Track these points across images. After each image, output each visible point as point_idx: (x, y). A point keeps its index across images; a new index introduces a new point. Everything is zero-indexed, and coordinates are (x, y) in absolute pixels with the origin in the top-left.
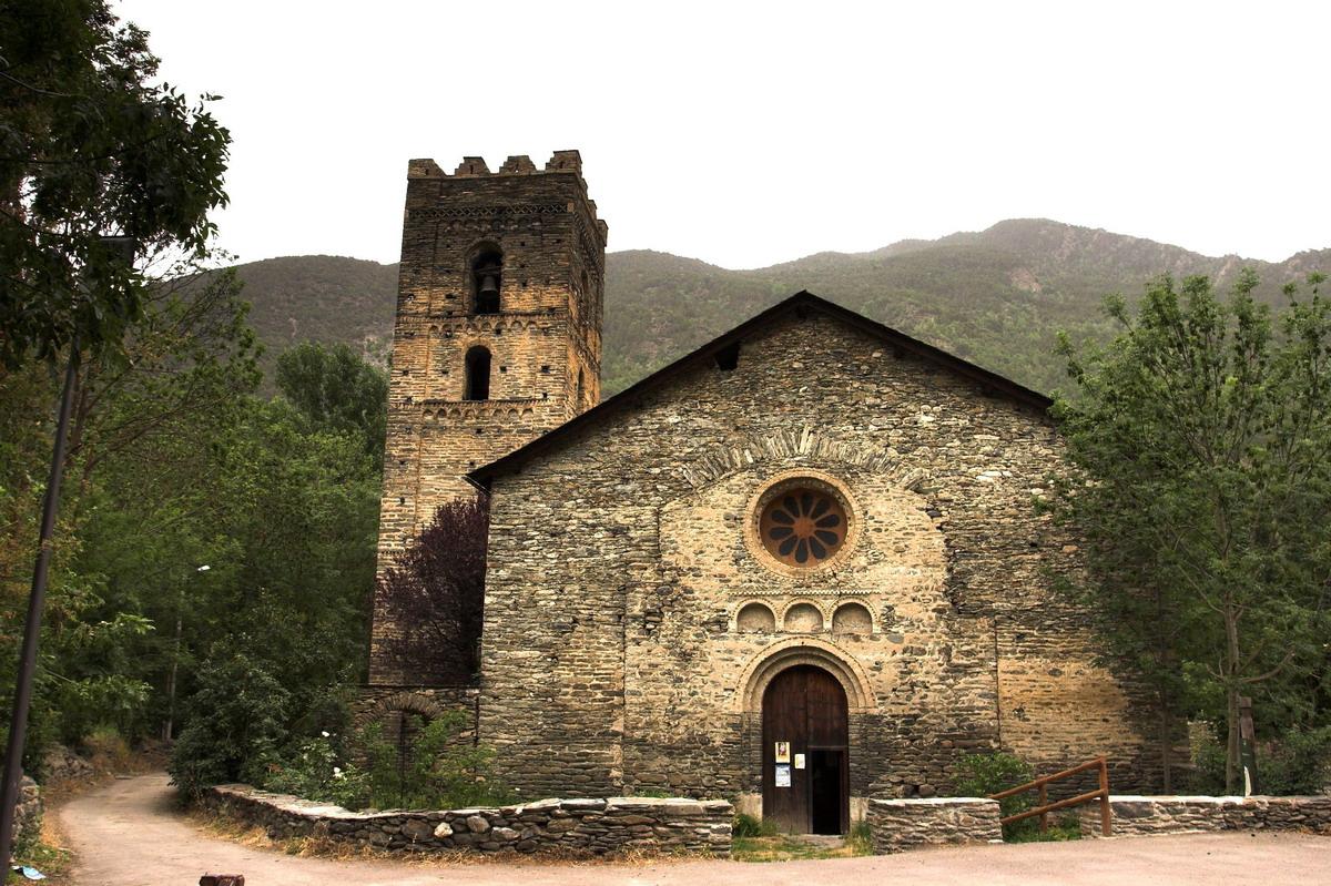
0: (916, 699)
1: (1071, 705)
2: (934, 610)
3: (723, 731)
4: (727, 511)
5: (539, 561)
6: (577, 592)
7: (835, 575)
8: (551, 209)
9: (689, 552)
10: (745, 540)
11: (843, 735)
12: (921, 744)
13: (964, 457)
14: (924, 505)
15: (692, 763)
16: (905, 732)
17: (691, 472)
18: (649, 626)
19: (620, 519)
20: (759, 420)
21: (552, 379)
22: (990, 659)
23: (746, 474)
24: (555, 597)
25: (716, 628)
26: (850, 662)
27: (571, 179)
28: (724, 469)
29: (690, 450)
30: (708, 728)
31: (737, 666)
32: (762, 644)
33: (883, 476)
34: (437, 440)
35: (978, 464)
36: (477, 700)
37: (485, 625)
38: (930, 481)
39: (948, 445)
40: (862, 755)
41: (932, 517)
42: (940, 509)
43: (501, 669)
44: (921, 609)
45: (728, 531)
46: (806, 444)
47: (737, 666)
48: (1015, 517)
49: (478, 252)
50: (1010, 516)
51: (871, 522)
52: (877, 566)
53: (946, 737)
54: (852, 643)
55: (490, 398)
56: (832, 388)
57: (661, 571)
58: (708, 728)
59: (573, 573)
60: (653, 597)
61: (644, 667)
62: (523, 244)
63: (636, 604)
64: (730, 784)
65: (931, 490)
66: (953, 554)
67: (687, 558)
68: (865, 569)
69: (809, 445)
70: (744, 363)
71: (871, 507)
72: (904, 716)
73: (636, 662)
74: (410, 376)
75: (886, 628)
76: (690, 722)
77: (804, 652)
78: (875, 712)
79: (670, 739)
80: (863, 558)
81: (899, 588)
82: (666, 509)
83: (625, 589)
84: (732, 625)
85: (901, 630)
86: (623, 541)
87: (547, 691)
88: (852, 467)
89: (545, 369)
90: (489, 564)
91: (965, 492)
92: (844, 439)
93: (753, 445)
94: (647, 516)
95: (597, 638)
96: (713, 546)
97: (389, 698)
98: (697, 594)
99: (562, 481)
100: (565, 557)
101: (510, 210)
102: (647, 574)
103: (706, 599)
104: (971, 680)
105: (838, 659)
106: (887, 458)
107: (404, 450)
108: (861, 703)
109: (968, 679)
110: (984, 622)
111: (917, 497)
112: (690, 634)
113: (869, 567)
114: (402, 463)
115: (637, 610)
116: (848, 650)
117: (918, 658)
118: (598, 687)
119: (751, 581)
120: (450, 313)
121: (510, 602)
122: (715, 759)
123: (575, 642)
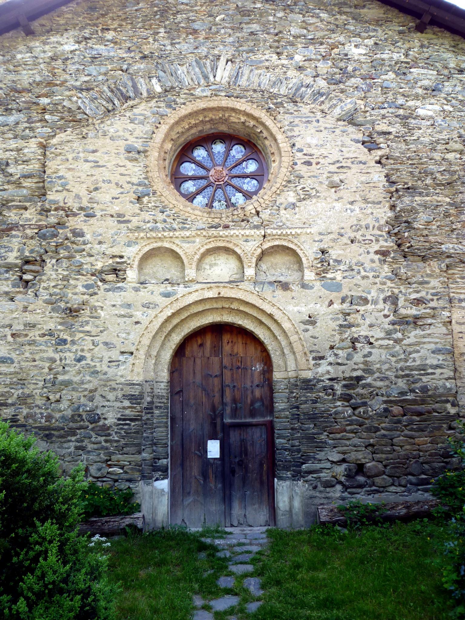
0: (358, 358)
2: (376, 252)
3: (118, 404)
4: (129, 142)
10: (150, 174)
11: (269, 406)
14: (360, 136)
15: (77, 448)
16: (346, 398)
17: (87, 101)
18: (26, 277)
20: (169, 48)
22: (444, 308)
23: (153, 103)
25: (111, 277)
28: (127, 98)
30: (98, 401)
31: (137, 323)
32: (167, 295)
35: (417, 97)
40: (292, 429)
41: (370, 150)
44: (361, 251)
45: (129, 164)
46: (224, 73)
47: (137, 323)
50: (455, 151)
51: (299, 155)
52: (308, 202)
54: (279, 293)
57: (45, 211)
58: (98, 401)
61: (18, 327)
63: (12, 251)
64: (126, 472)
65: (367, 122)
66: (395, 189)
67: (78, 196)
68: (294, 206)
69: (226, 74)
71: (299, 139)
72: (344, 379)
73: (7, 322)
75: (321, 274)
76: (75, 394)
77: (219, 305)
78: (309, 375)
79: (49, 418)
80: (292, 194)
81: (334, 228)
82: (54, 141)
84: (132, 274)
85: (339, 276)
88: (276, 96)
91: (405, 125)
92: (267, 68)
93: (161, 74)
94: (31, 148)
96: (110, 182)
102: (27, 215)
103: (100, 243)
104: (422, 333)
105: (263, 311)
106: (316, 88)
108: (291, 365)
109: (418, 332)
110: (434, 265)
111: (351, 129)
112: (79, 284)
113: (298, 204)
116: (274, 301)
117: (359, 308)
122: (106, 441)
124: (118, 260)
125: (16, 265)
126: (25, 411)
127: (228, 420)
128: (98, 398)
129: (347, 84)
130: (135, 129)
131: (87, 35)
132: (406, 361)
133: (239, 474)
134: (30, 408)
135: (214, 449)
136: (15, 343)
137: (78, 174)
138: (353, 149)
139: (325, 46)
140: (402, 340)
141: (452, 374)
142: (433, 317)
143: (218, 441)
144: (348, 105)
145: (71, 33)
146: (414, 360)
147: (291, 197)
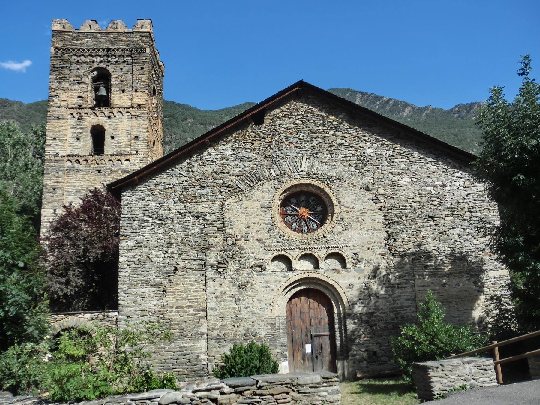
1: (454, 303)
2: (379, 254)
3: (266, 328)
4: (262, 203)
5: (153, 235)
6: (176, 252)
7: (325, 237)
8: (137, 51)
9: (241, 227)
12: (376, 328)
13: (391, 171)
17: (240, 182)
18: (220, 270)
19: (200, 209)
21: (140, 143)
22: (411, 280)
23: (272, 182)
24: (163, 256)
25: (259, 269)
26: (336, 285)
27: (148, 34)
29: (239, 169)
31: (272, 290)
32: (285, 277)
33: (348, 182)
34: (75, 176)
36: (117, 319)
37: (120, 274)
38: (373, 184)
39: (382, 164)
41: (376, 204)
42: (380, 199)
43: (131, 299)
47: (272, 290)
48: (420, 203)
49: (95, 73)
51: (343, 207)
52: (347, 231)
53: (389, 324)
54: (336, 274)
55: (105, 153)
56: (317, 135)
59: (173, 241)
60: (222, 253)
61: (218, 294)
62: (122, 69)
70: (267, 119)
71: (342, 199)
74: (57, 141)
75: (354, 265)
80: (340, 227)
82: (227, 202)
83: (204, 250)
86: (203, 222)
87: (160, 311)
89: (137, 137)
90: (121, 238)
91: (393, 190)
92: (326, 162)
94: (216, 207)
95: (189, 278)
97: (62, 321)
98: (247, 250)
99: (165, 188)
100: (168, 232)
101: (113, 50)
102: (217, 240)
104: (401, 291)
107: (55, 182)
111: (367, 193)
112: (244, 273)
114: (54, 189)
115: (212, 261)
118: (191, 307)
119: (278, 242)
120: (80, 106)
121: (135, 260)
123: (176, 281)
124: (261, 261)
125: (215, 265)
126: (223, 332)
127: (313, 334)
128: (256, 325)
129: (364, 169)
130: (264, 196)
131: (237, 146)
132: (394, 304)
133: (320, 358)
134: (226, 330)
135: (308, 348)
136: (217, 301)
137: (239, 220)
138: (368, 203)
139: (354, 149)
140: (392, 295)
141: (415, 310)
142: (406, 283)
143: (310, 345)
144: (366, 180)
145: (230, 144)
146: (398, 304)
147: (339, 228)
